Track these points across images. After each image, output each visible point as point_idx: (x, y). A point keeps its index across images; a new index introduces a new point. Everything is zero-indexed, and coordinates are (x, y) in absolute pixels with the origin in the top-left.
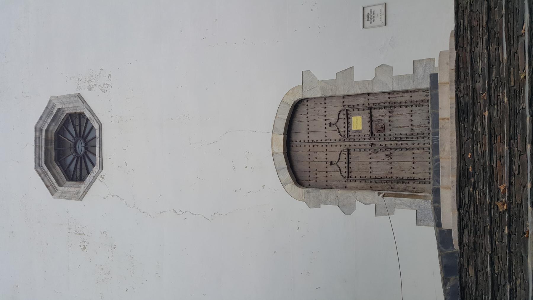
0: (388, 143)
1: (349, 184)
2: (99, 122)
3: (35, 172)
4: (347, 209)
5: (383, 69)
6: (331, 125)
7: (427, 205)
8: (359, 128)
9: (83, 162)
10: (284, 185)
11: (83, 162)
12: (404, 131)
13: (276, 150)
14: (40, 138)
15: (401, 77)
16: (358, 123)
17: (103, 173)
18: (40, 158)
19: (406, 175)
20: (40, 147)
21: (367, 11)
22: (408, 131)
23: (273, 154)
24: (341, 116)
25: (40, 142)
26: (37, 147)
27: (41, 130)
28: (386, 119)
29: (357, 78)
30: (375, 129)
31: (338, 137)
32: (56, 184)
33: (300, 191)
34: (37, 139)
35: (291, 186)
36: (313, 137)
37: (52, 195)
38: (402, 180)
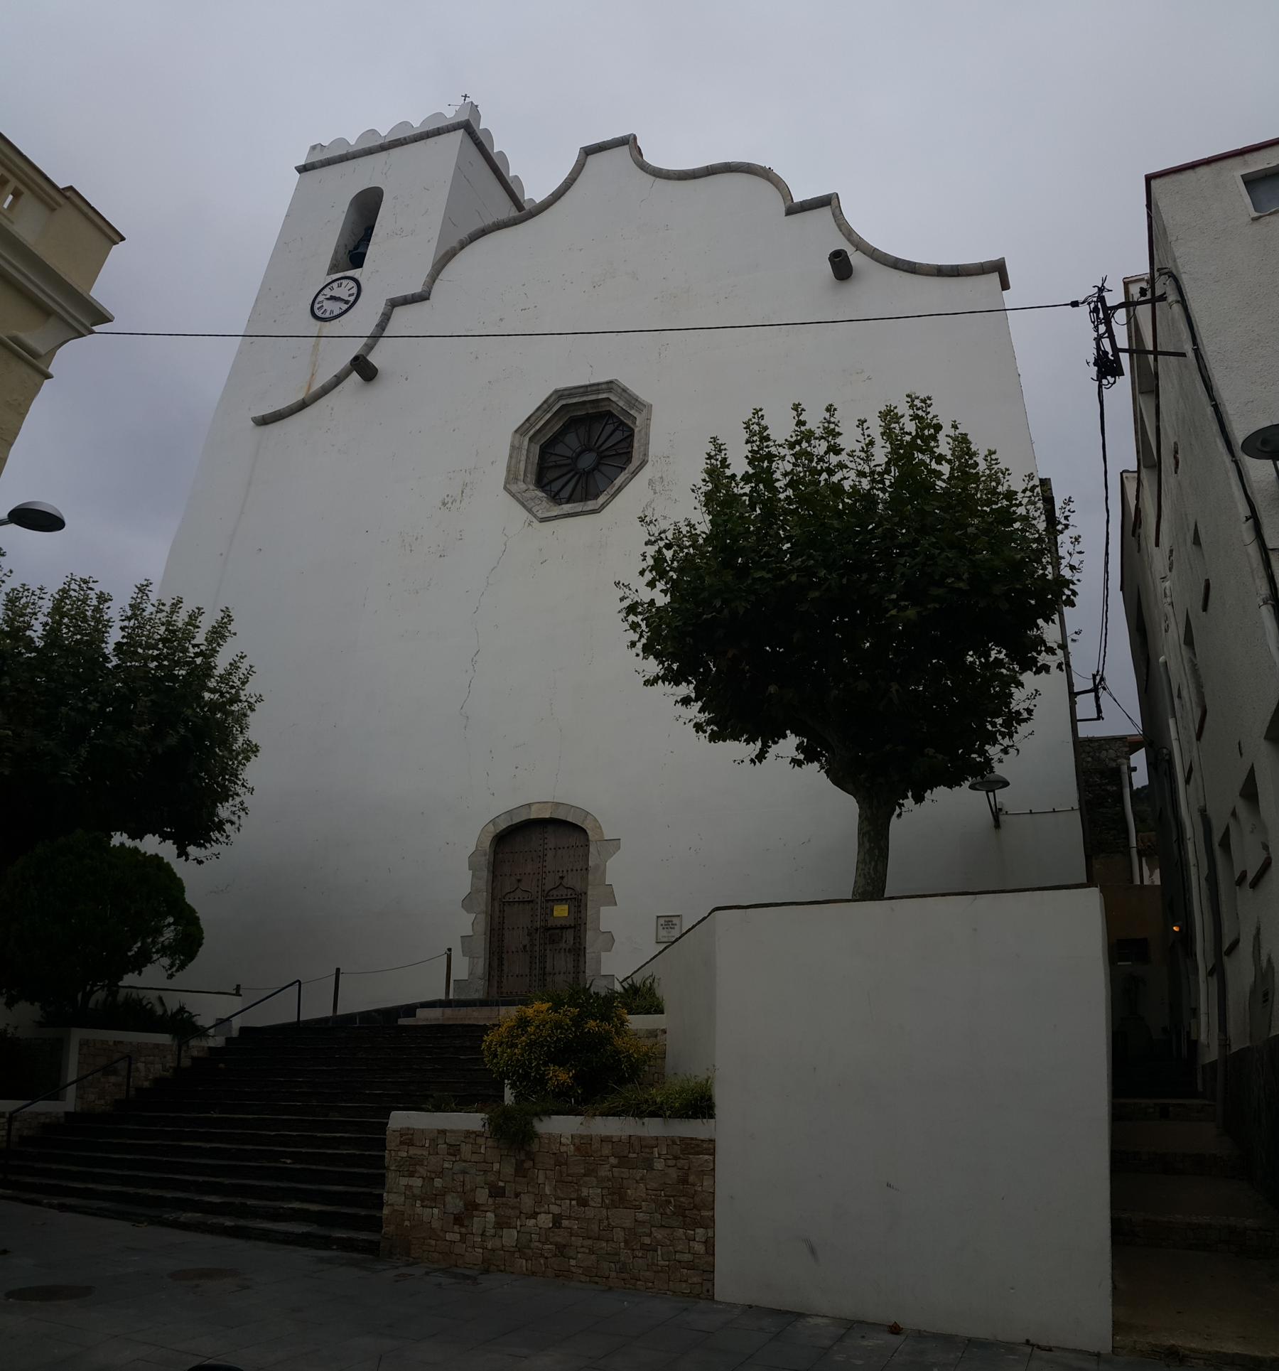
0: (537, 948)
1: (496, 905)
2: (603, 506)
3: (550, 392)
4: (467, 903)
5: (610, 939)
6: (562, 878)
7: (477, 992)
8: (555, 914)
9: (604, 447)
10: (493, 821)
11: (604, 447)
12: (549, 965)
13: (533, 808)
14: (598, 392)
15: (599, 962)
16: (561, 911)
17: (536, 523)
18: (570, 396)
19: (505, 968)
20: (585, 393)
21: (675, 920)
22: (549, 969)
23: (529, 805)
24: (570, 892)
25: (593, 392)
26: (586, 389)
27: (610, 390)
28: (563, 945)
29: (605, 911)
30: (552, 933)
31: (547, 888)
32: (532, 432)
33: (487, 844)
34: (595, 388)
35: (492, 831)
36: (550, 854)
37: (516, 431)
38: (501, 964)
